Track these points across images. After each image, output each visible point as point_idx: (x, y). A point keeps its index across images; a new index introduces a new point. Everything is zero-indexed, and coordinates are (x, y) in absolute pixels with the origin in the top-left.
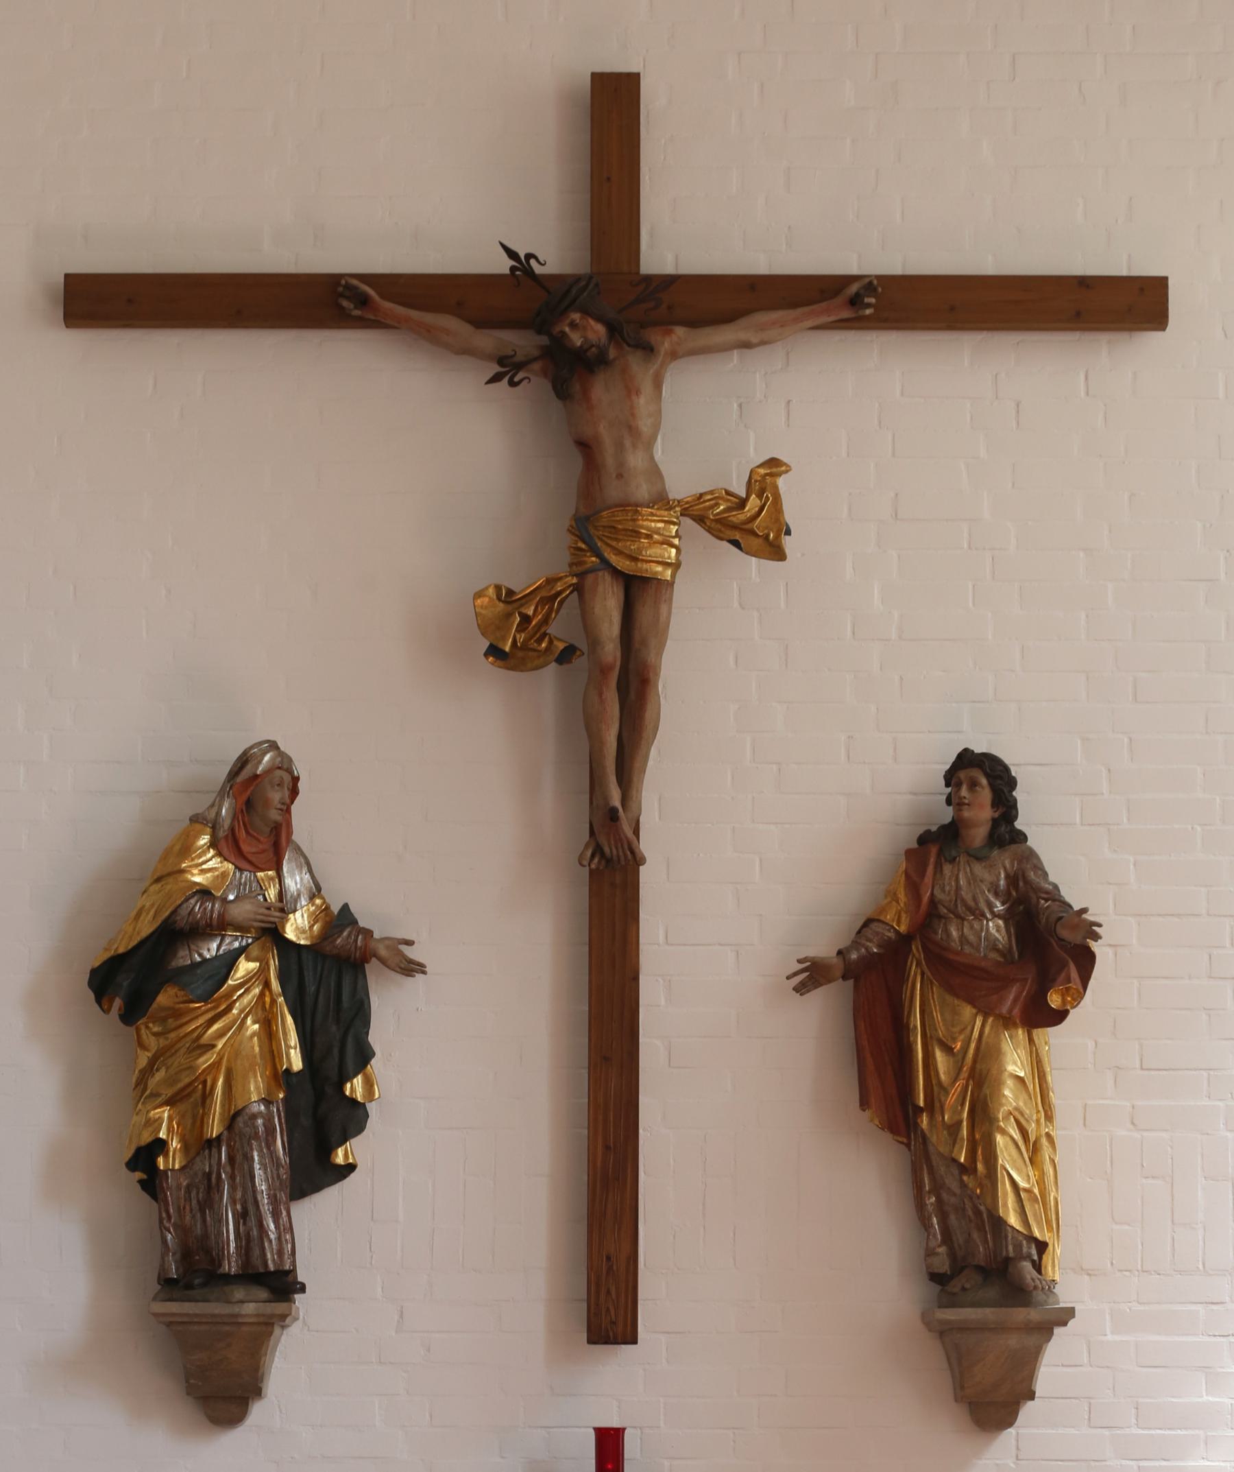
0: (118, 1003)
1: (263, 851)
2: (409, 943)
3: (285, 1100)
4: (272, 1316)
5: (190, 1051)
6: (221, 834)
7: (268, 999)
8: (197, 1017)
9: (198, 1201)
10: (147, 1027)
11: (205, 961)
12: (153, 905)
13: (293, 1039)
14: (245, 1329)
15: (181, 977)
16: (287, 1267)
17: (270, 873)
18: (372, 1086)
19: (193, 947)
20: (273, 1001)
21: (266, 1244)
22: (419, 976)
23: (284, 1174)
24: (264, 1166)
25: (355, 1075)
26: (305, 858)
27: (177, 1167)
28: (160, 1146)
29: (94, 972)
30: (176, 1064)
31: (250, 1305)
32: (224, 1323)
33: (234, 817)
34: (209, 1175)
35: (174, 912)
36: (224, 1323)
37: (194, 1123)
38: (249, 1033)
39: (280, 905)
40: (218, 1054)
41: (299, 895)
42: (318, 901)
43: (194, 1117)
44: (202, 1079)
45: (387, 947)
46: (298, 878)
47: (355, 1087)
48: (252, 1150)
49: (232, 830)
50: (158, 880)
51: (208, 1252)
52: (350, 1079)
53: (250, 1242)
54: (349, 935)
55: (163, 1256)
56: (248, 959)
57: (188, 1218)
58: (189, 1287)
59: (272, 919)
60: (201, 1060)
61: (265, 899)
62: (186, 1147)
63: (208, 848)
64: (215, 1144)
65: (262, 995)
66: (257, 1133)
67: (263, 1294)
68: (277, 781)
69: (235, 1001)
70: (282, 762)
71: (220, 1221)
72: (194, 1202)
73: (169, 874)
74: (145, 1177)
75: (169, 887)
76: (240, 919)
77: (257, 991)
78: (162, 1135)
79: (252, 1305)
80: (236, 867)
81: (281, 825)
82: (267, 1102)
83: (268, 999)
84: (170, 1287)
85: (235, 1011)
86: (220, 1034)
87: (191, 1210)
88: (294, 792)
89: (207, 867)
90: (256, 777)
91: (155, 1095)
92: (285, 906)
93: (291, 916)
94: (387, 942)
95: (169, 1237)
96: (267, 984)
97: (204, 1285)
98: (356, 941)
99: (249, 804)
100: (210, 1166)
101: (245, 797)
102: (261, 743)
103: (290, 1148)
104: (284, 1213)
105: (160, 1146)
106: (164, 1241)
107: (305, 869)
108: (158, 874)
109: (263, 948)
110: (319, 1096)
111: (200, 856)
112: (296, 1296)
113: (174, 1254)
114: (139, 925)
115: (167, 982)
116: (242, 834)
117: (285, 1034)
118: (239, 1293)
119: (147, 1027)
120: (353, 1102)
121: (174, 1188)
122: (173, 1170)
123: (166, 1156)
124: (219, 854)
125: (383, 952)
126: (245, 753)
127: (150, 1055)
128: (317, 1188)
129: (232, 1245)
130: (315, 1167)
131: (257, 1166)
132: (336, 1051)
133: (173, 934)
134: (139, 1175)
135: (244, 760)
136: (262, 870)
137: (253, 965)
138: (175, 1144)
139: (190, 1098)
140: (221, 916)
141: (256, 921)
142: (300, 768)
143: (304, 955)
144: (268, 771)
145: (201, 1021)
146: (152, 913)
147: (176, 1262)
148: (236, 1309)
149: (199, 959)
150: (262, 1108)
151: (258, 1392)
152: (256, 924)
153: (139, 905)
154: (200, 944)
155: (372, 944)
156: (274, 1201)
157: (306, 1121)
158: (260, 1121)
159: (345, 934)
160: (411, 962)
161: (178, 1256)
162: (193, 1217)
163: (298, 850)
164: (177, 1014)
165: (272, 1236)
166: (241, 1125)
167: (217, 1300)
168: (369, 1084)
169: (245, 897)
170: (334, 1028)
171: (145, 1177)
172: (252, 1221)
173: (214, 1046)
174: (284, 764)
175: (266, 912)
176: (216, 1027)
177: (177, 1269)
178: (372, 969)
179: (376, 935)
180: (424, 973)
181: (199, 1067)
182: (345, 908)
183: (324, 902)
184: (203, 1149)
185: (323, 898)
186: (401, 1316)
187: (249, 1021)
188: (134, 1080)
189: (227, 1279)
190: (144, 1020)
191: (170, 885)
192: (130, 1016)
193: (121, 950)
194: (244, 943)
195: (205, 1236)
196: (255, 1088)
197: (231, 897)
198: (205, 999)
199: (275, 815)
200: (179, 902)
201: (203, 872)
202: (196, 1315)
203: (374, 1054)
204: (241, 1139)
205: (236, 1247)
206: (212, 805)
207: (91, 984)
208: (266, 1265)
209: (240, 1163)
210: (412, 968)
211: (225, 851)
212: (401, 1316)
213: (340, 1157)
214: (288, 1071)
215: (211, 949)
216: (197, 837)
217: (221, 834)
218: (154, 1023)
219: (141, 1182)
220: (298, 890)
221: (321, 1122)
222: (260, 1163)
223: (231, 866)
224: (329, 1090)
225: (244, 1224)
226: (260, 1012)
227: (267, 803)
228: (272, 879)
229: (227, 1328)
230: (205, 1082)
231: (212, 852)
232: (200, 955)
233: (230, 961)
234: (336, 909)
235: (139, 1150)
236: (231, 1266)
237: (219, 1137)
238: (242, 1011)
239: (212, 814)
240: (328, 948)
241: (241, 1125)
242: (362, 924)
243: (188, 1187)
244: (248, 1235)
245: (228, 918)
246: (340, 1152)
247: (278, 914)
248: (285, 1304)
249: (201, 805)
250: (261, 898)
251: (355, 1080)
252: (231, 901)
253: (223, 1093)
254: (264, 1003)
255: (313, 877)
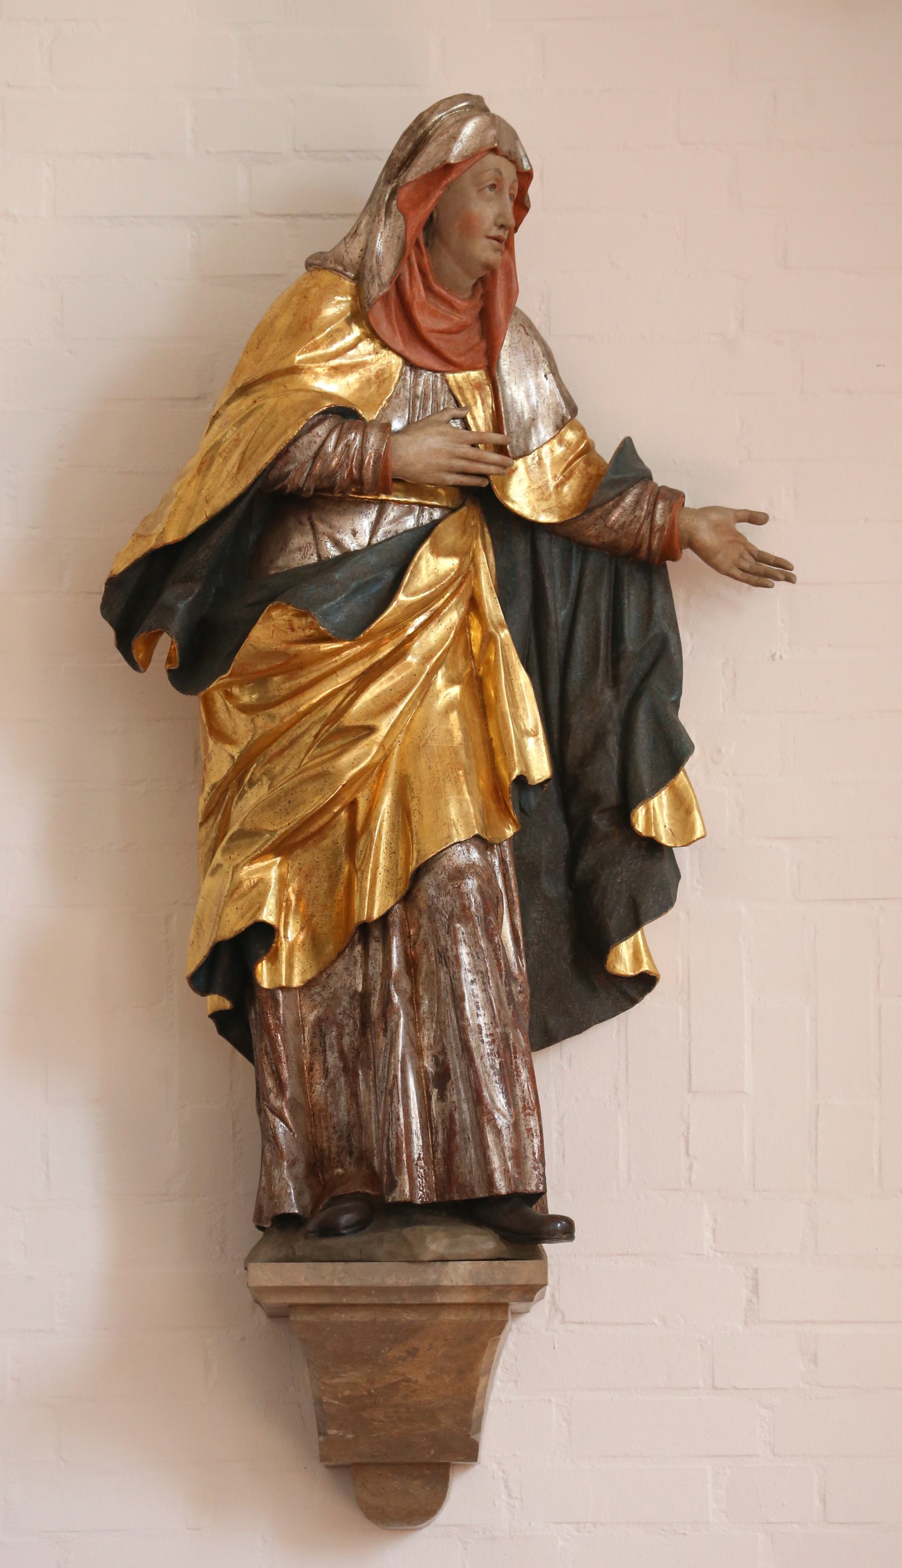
0: (165, 645)
1: (461, 328)
2: (756, 519)
3: (515, 842)
4: (506, 1289)
5: (320, 741)
6: (375, 291)
7: (476, 634)
8: (334, 672)
9: (341, 1053)
10: (228, 695)
11: (347, 556)
12: (237, 441)
13: (530, 714)
14: (449, 1317)
15: (293, 588)
16: (532, 1188)
17: (474, 374)
18: (688, 812)
19: (321, 527)
20: (489, 639)
21: (490, 1138)
22: (781, 586)
23: (521, 991)
24: (482, 976)
25: (655, 791)
26: (543, 344)
27: (297, 982)
28: (261, 937)
29: (114, 584)
30: (292, 768)
31: (458, 1264)
32: (405, 1307)
33: (402, 256)
34: (364, 998)
35: (283, 455)
36: (405, 1307)
37: (332, 890)
38: (436, 713)
39: (497, 438)
40: (382, 745)
41: (533, 420)
42: (570, 435)
43: (333, 877)
44: (348, 798)
45: (716, 527)
46: (532, 384)
47: (655, 816)
48: (456, 942)
49: (398, 283)
50: (244, 390)
51: (363, 1158)
52: (643, 798)
53: (448, 1142)
54: (637, 503)
55: (267, 1168)
56: (437, 552)
57: (318, 1088)
58: (329, 1230)
59: (483, 468)
60: (346, 759)
61: (467, 427)
62: (314, 942)
63: (349, 321)
64: (376, 933)
65: (463, 627)
66: (465, 908)
67: (487, 1243)
68: (489, 177)
69: (411, 638)
70: (496, 139)
71: (389, 1092)
72: (332, 1058)
73: (268, 378)
74: (227, 1005)
75: (270, 402)
76: (419, 467)
77: (452, 618)
78: (268, 915)
79: (464, 1267)
80: (407, 362)
81: (493, 272)
82: (483, 843)
83: (476, 634)
84: (281, 1230)
85: (412, 659)
86: (385, 706)
87: (326, 1072)
88: (521, 206)
89: (348, 366)
90: (447, 168)
91: (247, 834)
92: (506, 441)
93: (519, 463)
94: (714, 517)
95: (281, 1128)
96: (474, 605)
97: (360, 1226)
98: (652, 514)
99: (431, 226)
100: (366, 978)
101: (422, 214)
102: (453, 100)
103: (527, 942)
104: (524, 1075)
105: (261, 937)
106: (269, 1137)
107: (544, 367)
108: (244, 378)
109: (464, 529)
110: (579, 835)
111: (331, 338)
112: (548, 1248)
113: (292, 1164)
114: (209, 482)
115: (272, 600)
116: (417, 293)
117: (514, 704)
118: (436, 1241)
119: (228, 695)
120: (652, 846)
121: (290, 1027)
122: (287, 989)
123: (274, 959)
124: (372, 334)
125: (707, 536)
126: (420, 121)
127: (235, 752)
128: (577, 1027)
129: (417, 1142)
130: (579, 975)
131: (467, 976)
132: (613, 742)
133: (277, 501)
134: (216, 1002)
135: (417, 138)
136: (460, 368)
137: (449, 564)
138: (291, 933)
139: (325, 838)
140: (382, 460)
141: (451, 471)
142: (534, 155)
143: (544, 543)
144: (471, 158)
145: (342, 679)
146: (235, 458)
147: (295, 1179)
148: (429, 1276)
149: (334, 552)
150: (475, 855)
151: (470, 1452)
152: (452, 479)
153: (207, 443)
154: (337, 521)
155: (685, 522)
156: (504, 1048)
157: (553, 888)
158: (471, 884)
159: (629, 499)
160: (761, 558)
161: (300, 1168)
162: (331, 1085)
163: (528, 327)
164: (291, 665)
165: (502, 1122)
166: (432, 891)
167: (392, 1257)
168: (683, 808)
169: (427, 422)
170: (608, 695)
171: (227, 1005)
172: (459, 1093)
173: (371, 730)
174: (502, 145)
175: (472, 452)
176: (368, 696)
177: (299, 1195)
178: (685, 575)
179: (688, 504)
180: (790, 579)
181: (341, 774)
182: (626, 448)
183: (584, 436)
184: (351, 945)
185: (580, 429)
186: (755, 1290)
187: (440, 680)
188: (202, 806)
189: (407, 1212)
190: (223, 679)
191: (270, 398)
192: (193, 671)
193: (172, 537)
194: (425, 520)
195: (358, 1124)
196: (457, 816)
197: (397, 425)
198: (354, 630)
199: (485, 251)
200: (292, 433)
201: (337, 371)
202: (347, 1290)
203: (693, 747)
204: (432, 920)
205: (425, 1147)
206: (354, 233)
207: (107, 608)
208: (490, 1181)
209: (428, 969)
210: (766, 571)
211: (384, 329)
212: (755, 1290)
213: (623, 960)
214: (522, 782)
215: (358, 531)
216: (323, 300)
217: (375, 291)
218: (241, 685)
219: (217, 1017)
220: (534, 411)
221: (586, 885)
222: (476, 971)
223: (395, 361)
224: (601, 822)
225: (442, 1097)
226: (461, 662)
227: (468, 226)
228: (478, 387)
229: (409, 1317)
230: (353, 806)
231: (356, 331)
232: (337, 544)
233: (401, 555)
234: (606, 451)
235: (217, 949)
236: (414, 1185)
237: (384, 919)
238: (426, 659)
239: (354, 251)
240: (592, 532)
241: (432, 891)
242: (660, 479)
243: (320, 1025)
244: (450, 1121)
245: (396, 465)
246: (625, 949)
247: (496, 457)
248: (530, 1264)
249: (326, 239)
250: (457, 424)
251: (654, 802)
252: (398, 432)
253: (393, 828)
254: (468, 644)
255: (560, 385)
